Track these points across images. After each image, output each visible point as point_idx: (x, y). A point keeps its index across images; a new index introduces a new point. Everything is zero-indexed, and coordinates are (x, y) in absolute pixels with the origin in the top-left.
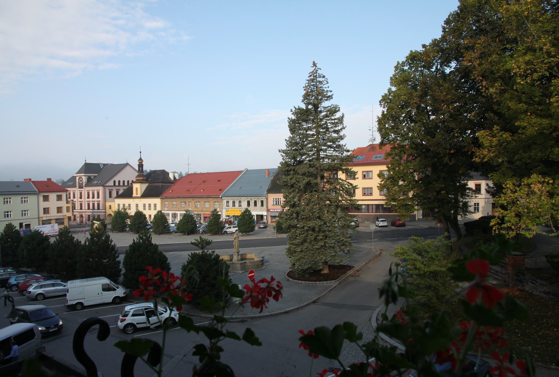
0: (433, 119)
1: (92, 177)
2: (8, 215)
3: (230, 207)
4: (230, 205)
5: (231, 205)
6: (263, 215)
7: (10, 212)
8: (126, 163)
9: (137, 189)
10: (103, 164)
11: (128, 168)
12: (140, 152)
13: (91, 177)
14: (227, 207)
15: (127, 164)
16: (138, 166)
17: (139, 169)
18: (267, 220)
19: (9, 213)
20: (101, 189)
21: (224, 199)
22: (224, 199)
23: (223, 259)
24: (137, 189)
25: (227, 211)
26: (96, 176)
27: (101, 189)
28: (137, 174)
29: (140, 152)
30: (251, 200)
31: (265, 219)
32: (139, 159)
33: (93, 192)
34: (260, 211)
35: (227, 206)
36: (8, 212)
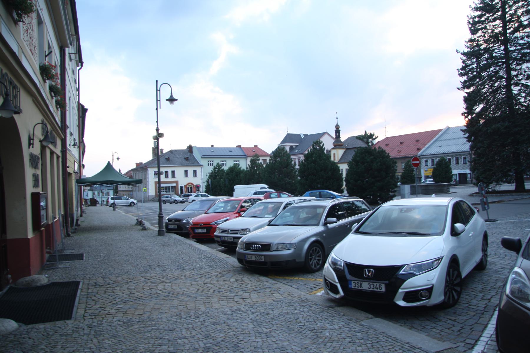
0: (504, 59)
1: (294, 147)
2: (211, 164)
3: (429, 167)
4: (428, 164)
5: (430, 164)
6: (466, 173)
7: (213, 162)
8: (363, 134)
9: (334, 154)
10: (304, 135)
11: (326, 135)
12: (337, 118)
13: (293, 147)
14: (426, 167)
15: (326, 133)
16: (335, 132)
17: (336, 135)
18: (471, 179)
19: (212, 163)
20: (301, 157)
21: (423, 158)
22: (423, 158)
23: (46, 82)
24: (334, 154)
25: (425, 171)
26: (297, 146)
27: (301, 157)
28: (333, 141)
29: (337, 118)
30: (452, 157)
31: (469, 178)
32: (336, 125)
33: (299, 160)
34: (463, 169)
35: (425, 166)
36: (464, 347)
